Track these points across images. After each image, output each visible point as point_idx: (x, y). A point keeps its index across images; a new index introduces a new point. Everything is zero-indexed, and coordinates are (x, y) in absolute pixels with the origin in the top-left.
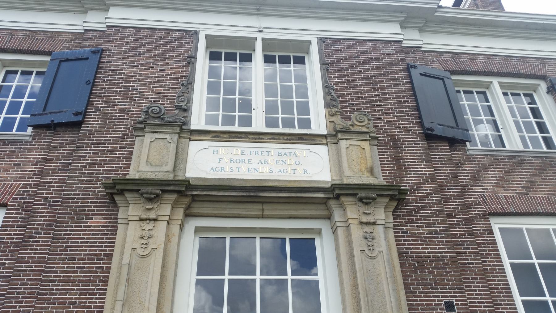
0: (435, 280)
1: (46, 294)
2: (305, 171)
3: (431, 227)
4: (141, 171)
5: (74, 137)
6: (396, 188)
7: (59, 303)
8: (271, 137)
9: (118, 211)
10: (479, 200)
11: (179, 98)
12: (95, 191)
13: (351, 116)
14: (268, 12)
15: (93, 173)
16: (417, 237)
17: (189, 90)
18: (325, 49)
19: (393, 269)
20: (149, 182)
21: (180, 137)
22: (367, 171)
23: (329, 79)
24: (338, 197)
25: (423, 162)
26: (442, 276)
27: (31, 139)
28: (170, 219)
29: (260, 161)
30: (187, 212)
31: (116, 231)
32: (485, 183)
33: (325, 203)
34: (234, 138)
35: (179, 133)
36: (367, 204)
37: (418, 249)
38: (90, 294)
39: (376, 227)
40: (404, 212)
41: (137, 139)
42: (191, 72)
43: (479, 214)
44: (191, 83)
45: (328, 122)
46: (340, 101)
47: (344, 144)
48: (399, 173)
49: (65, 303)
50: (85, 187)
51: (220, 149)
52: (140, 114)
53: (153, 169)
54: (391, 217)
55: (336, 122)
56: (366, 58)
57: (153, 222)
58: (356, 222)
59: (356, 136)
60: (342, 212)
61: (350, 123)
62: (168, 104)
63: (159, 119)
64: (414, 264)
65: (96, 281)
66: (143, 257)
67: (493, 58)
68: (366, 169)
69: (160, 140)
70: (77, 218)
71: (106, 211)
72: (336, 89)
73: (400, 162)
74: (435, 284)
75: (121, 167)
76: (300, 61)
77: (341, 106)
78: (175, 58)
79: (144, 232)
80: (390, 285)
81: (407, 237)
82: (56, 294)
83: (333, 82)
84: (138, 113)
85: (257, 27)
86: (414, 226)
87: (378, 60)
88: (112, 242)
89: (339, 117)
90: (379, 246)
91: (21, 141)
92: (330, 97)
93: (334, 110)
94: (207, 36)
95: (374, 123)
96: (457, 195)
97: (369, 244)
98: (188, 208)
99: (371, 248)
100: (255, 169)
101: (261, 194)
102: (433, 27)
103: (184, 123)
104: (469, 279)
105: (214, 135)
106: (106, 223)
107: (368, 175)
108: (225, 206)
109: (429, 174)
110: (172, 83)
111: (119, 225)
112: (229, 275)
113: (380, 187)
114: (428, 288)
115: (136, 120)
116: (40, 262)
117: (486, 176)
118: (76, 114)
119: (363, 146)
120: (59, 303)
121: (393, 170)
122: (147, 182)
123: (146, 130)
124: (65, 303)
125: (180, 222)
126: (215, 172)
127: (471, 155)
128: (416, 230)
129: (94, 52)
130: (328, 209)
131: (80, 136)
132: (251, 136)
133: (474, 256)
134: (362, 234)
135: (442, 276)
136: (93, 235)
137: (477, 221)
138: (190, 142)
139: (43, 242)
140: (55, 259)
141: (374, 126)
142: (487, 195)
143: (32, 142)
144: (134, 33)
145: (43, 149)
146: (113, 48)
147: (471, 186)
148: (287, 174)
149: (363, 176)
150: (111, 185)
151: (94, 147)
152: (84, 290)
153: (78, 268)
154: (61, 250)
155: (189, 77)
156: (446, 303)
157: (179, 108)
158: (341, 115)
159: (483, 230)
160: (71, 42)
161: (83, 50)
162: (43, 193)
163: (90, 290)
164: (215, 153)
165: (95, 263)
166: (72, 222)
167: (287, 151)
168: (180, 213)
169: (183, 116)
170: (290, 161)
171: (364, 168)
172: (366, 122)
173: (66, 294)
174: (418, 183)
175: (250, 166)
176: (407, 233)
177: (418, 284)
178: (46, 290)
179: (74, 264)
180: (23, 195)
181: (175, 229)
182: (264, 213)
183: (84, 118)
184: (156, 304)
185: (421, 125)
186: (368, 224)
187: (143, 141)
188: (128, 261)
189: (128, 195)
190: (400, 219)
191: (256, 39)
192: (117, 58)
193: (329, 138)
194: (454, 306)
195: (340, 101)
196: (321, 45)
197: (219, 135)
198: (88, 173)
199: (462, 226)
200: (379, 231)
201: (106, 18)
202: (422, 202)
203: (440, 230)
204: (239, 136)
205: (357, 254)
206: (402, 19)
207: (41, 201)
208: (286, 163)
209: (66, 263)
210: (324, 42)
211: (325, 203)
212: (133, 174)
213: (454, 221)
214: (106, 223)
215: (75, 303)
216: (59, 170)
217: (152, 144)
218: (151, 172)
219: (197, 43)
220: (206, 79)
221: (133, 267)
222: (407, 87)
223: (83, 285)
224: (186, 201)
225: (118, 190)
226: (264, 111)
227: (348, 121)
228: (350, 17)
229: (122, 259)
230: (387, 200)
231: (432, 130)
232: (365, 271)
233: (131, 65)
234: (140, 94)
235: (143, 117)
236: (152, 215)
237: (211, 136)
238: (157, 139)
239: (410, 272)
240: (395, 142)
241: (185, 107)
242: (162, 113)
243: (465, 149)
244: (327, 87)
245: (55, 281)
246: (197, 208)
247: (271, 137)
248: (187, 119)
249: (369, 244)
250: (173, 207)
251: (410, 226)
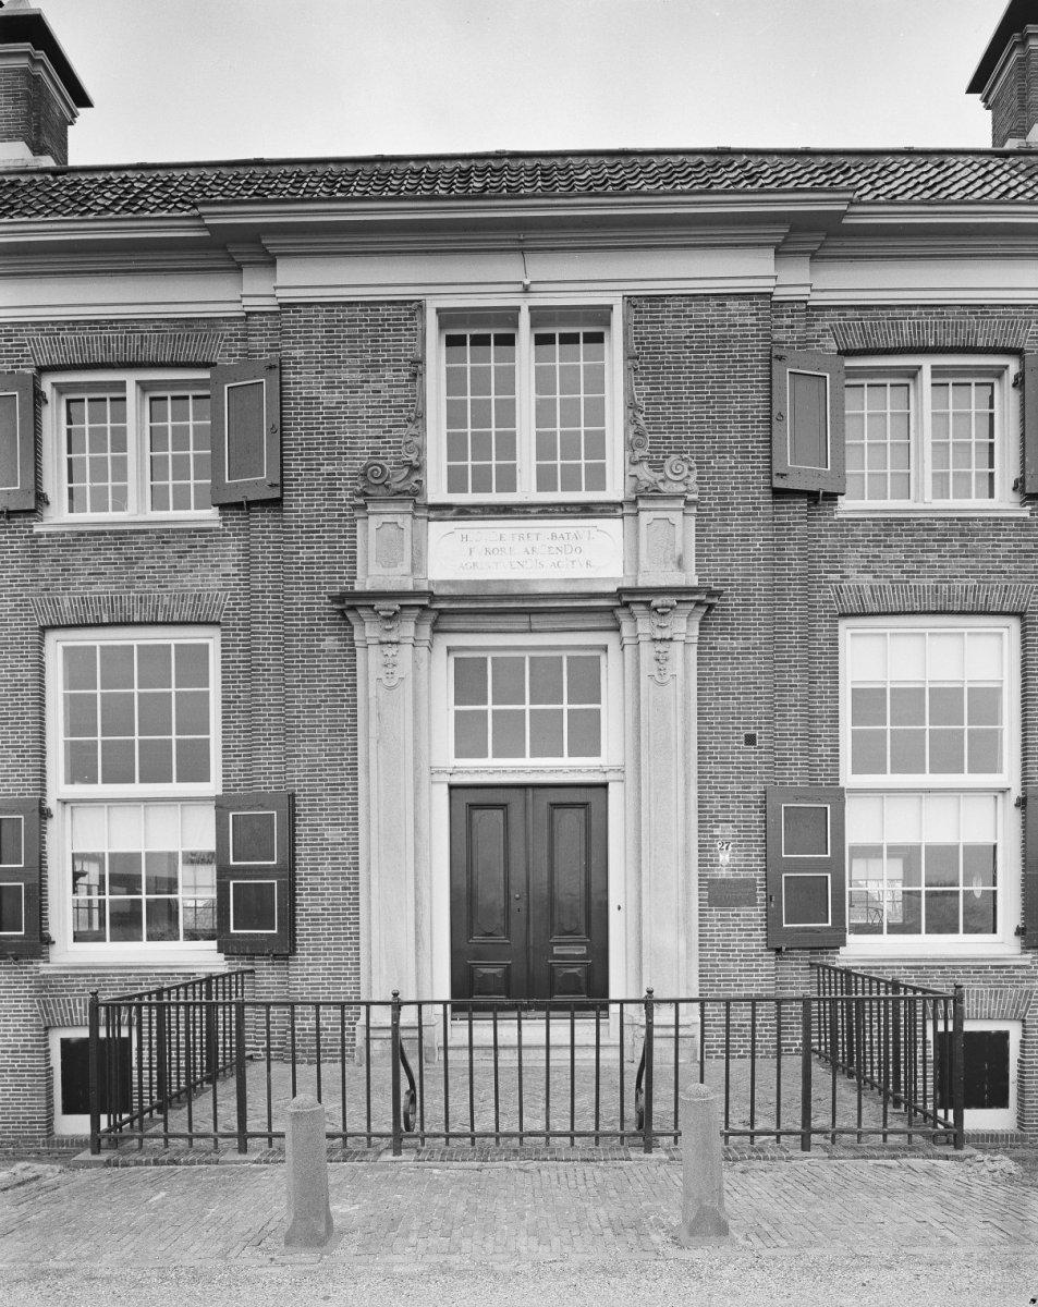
9: (352, 629)
33: (612, 611)
39: (672, 644)
45: (627, 476)
56: (703, 337)
58: (647, 638)
66: (391, 688)
67: (937, 313)
76: (597, 338)
78: (393, 366)
87: (724, 340)
91: (210, 530)
92: (635, 426)
98: (435, 623)
103: (417, 493)
107: (674, 567)
110: (393, 416)
115: (352, 489)
117: (853, 557)
127: (839, 519)
130: (616, 620)
143: (223, 530)
146: (298, 353)
152: (333, 726)
158: (650, 462)
162: (258, 607)
163: (339, 725)
167: (564, 531)
168: (426, 630)
172: (686, 472)
176: (715, 648)
181: (423, 652)
186: (663, 640)
201: (275, 288)
205: (644, 680)
206: (779, 239)
219: (424, 330)
220: (444, 397)
227: (658, 472)
229: (368, 691)
230: (692, 606)
233: (330, 387)
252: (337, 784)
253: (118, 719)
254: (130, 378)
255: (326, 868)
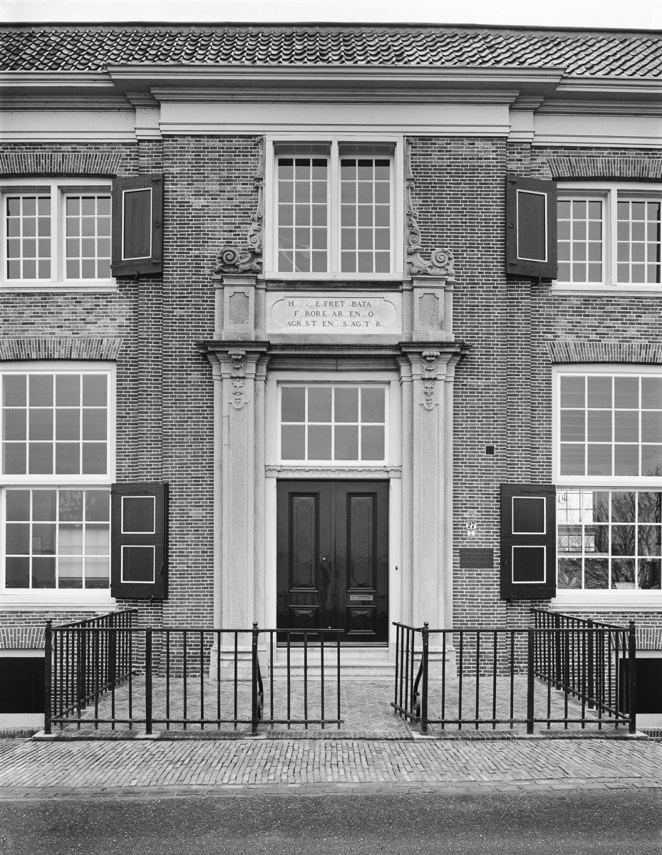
7: (179, 446)
10: (547, 348)
27: (118, 292)
40: (468, 365)
41: (217, 292)
45: (405, 263)
47: (418, 293)
51: (295, 299)
54: (454, 370)
58: (419, 377)
60: (409, 367)
66: (238, 410)
86: (474, 379)
98: (270, 363)
112: (282, 459)
117: (562, 322)
125: (264, 378)
146: (175, 170)
147: (544, 333)
158: (421, 253)
176: (466, 385)
180: (126, 351)
181: (261, 384)
191: (331, 142)
206: (513, 100)
224: (267, 359)
230: (450, 356)
233: (197, 194)
250: (257, 365)
253: (41, 429)
254: (54, 184)
255: (190, 537)
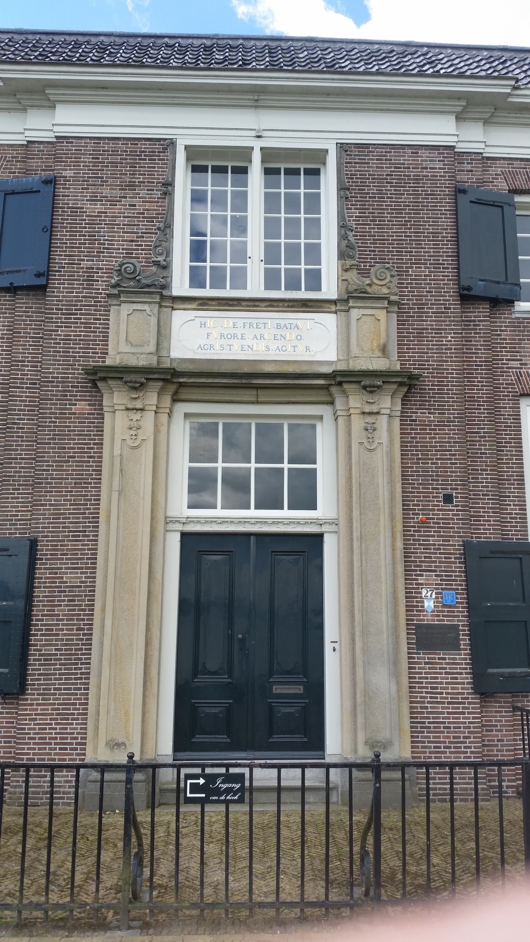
0: (438, 472)
1: (42, 483)
2: (307, 349)
3: (444, 414)
4: (122, 353)
5: (40, 304)
6: (405, 374)
7: (56, 492)
8: (268, 304)
9: (102, 396)
10: (513, 378)
11: (156, 250)
12: (74, 374)
13: (370, 269)
14: (269, 103)
15: (69, 352)
16: (426, 425)
17: (168, 236)
18: (346, 163)
19: (391, 461)
20: (132, 370)
21: (161, 306)
22: (379, 350)
23: (348, 213)
24: (340, 384)
25: (450, 333)
26: (445, 467)
28: (157, 407)
29: (255, 336)
30: (175, 397)
31: (103, 419)
32: (526, 356)
33: (327, 388)
34: (224, 305)
35: (159, 303)
36: (371, 392)
37: (426, 438)
38: (85, 483)
39: (379, 417)
40: (417, 397)
41: (112, 308)
42: (168, 208)
43: (508, 396)
44: (170, 226)
45: (340, 281)
46: (359, 247)
47: (355, 313)
48: (419, 349)
49: (62, 492)
50: (63, 369)
52: (111, 273)
53: (134, 350)
55: (350, 280)
57: (140, 411)
58: (358, 411)
59: (371, 303)
61: (368, 281)
62: (143, 258)
63: (134, 281)
64: (418, 455)
65: (89, 470)
68: (378, 346)
69: (139, 312)
70: (60, 404)
71: (90, 396)
72: (356, 228)
73: (423, 333)
74: (437, 476)
75: (98, 345)
77: (359, 254)
79: (132, 423)
80: (385, 478)
81: (415, 425)
82: (51, 483)
83: (352, 217)
84: (109, 271)
85: (255, 130)
86: (425, 413)
87: (417, 179)
88: (100, 430)
89: (355, 272)
90: (380, 438)
92: (346, 242)
93: (349, 262)
94: (186, 147)
95: (399, 279)
96: (485, 374)
97: (369, 435)
98: (176, 393)
99: (371, 440)
100: (249, 346)
101: (254, 381)
102: (505, 117)
104: (477, 470)
105: (200, 302)
106: (91, 410)
107: (379, 354)
108: (214, 392)
109: (455, 349)
111: (106, 414)
113: (387, 374)
114: (428, 480)
116: (29, 450)
118: (39, 275)
119: (379, 315)
120: (56, 492)
121: (413, 345)
122: (129, 370)
123: (122, 299)
124: (62, 492)
125: (168, 411)
126: (204, 351)
128: (427, 417)
129: (46, 182)
130: (331, 395)
131: (47, 305)
132: (244, 303)
133: (489, 445)
134: (363, 425)
135: (445, 467)
136: (79, 422)
137: (503, 403)
138: (174, 312)
139: (27, 428)
140: (45, 448)
141: (399, 283)
142: (524, 372)
144: (92, 147)
145: (6, 317)
146: (68, 173)
147: (507, 360)
148: (286, 352)
149: (373, 356)
150: (92, 371)
151: (65, 318)
152: (79, 479)
153: (69, 457)
154: (49, 439)
155: (167, 217)
156: (444, 495)
157: (157, 264)
159: (508, 415)
160: (13, 161)
161: (31, 179)
164: (203, 326)
165: (86, 453)
166: (56, 409)
168: (167, 400)
169: (162, 276)
170: (291, 335)
171: (375, 345)
173: (61, 483)
174: (439, 361)
175: (243, 342)
177: (417, 476)
178: (41, 479)
179: (64, 453)
181: (164, 418)
182: (259, 400)
183: (48, 279)
184: (150, 495)
185: (458, 280)
186: (370, 414)
187: (119, 312)
188: (119, 452)
189: (110, 382)
190: (411, 405)
192: (74, 189)
193: (338, 304)
194: (452, 499)
195: (359, 247)
196: (340, 158)
197: (206, 302)
198: (63, 352)
199: (483, 412)
200: (383, 421)
201: (53, 125)
202: (440, 384)
203: (454, 418)
204: (231, 303)
207: (17, 383)
208: (285, 339)
209: (56, 453)
210: (346, 151)
211: (327, 388)
212: (109, 362)
213: (474, 405)
214: (91, 410)
215: (72, 491)
216: (30, 345)
217: (130, 317)
218: (133, 353)
219: (174, 160)
221: (125, 457)
222: (450, 222)
223: (76, 475)
225: (100, 377)
226: (262, 261)
227: (365, 277)
228: (385, 107)
231: (469, 289)
232: (362, 463)
233: (94, 200)
234: (108, 244)
235: (117, 279)
236: (139, 405)
237: (197, 303)
238: (135, 312)
239: (411, 463)
240: (421, 306)
241: (164, 263)
242: (138, 273)
243: (510, 310)
244: (343, 226)
245: (48, 470)
246: (184, 394)
247: (268, 304)
248: (167, 279)
249: (369, 435)
251: (421, 413)
252: (80, 531)
